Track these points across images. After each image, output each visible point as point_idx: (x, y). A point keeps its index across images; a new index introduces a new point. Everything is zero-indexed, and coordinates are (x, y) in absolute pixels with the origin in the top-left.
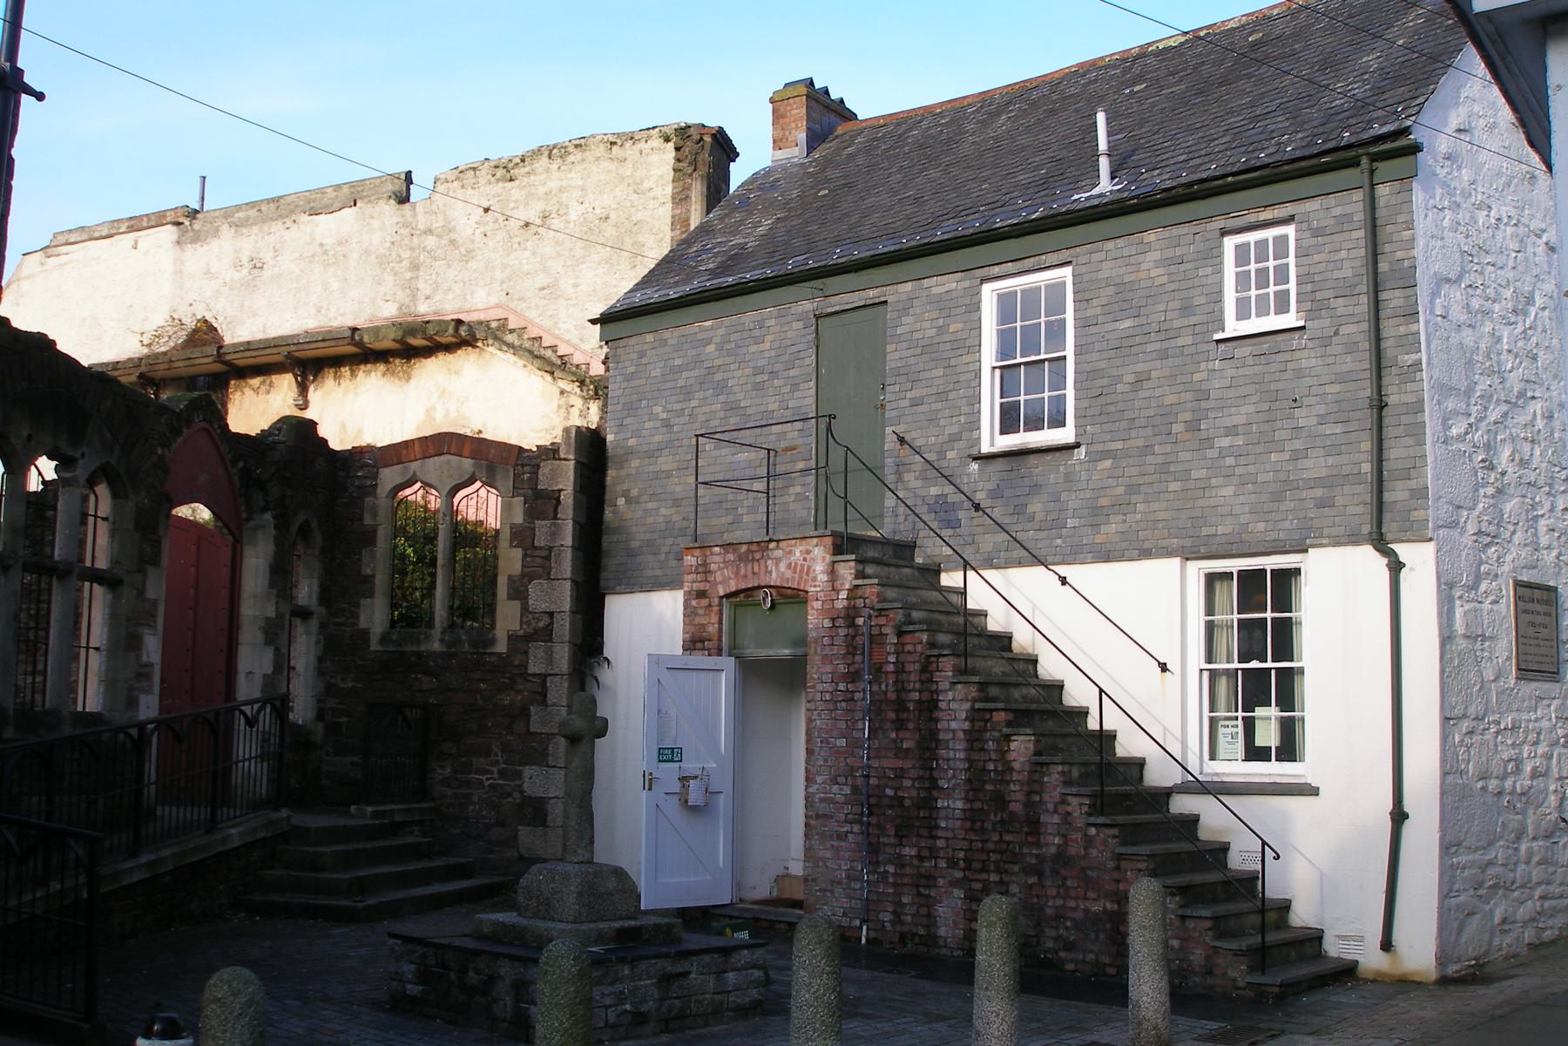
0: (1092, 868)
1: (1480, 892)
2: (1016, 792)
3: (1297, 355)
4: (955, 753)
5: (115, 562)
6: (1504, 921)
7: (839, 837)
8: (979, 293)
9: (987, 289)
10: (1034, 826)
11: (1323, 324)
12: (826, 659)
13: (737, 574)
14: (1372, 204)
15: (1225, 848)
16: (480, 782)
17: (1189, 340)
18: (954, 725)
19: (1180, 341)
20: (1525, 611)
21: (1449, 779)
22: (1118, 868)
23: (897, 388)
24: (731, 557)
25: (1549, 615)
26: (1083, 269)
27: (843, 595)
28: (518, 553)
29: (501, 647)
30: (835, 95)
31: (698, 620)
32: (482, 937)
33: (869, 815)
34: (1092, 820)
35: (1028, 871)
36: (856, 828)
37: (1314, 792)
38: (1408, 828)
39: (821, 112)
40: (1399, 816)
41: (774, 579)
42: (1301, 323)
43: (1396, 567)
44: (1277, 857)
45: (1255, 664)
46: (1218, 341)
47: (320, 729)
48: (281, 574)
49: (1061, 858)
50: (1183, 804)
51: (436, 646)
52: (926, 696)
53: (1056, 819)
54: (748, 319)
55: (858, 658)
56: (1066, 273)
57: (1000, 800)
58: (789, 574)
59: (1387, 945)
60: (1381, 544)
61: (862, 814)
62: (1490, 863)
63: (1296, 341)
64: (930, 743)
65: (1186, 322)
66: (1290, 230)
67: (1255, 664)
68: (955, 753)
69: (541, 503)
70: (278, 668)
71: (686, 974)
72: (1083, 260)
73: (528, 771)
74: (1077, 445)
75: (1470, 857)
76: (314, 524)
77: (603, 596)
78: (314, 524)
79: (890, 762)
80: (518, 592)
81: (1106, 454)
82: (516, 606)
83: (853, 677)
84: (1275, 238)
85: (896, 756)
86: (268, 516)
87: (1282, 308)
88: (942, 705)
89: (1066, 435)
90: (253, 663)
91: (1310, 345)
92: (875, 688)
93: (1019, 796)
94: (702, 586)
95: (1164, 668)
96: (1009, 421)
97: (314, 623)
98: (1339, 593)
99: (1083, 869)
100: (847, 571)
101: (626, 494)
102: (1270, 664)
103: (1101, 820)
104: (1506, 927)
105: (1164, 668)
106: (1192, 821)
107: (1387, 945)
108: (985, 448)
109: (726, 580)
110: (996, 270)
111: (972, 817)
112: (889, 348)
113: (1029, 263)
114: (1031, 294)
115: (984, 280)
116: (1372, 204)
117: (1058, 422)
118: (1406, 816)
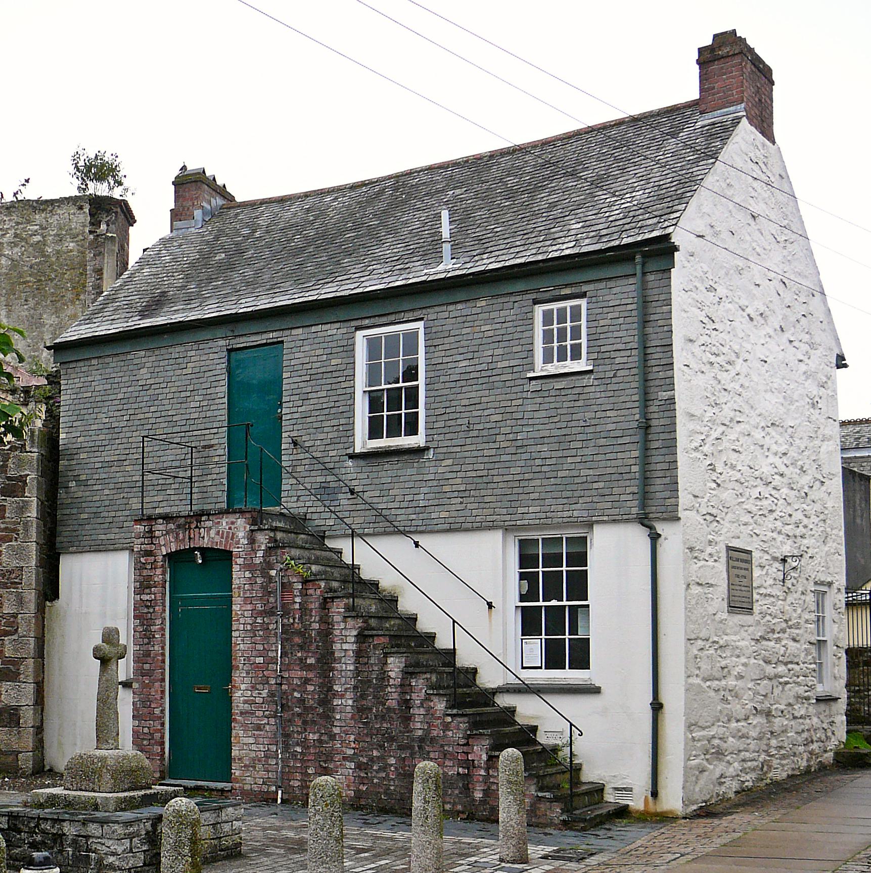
0: (449, 745)
1: (707, 757)
3: (586, 390)
4: (346, 666)
6: (721, 776)
9: (360, 334)
10: (407, 719)
12: (247, 600)
13: (177, 538)
14: (644, 286)
18: (345, 647)
20: (733, 567)
21: (690, 680)
22: (467, 744)
23: (291, 404)
25: (747, 569)
26: (431, 324)
27: (260, 554)
30: (709, 42)
31: (145, 573)
32: (41, 806)
33: (282, 712)
34: (449, 712)
35: (401, 748)
36: (272, 721)
37: (596, 691)
40: (657, 707)
41: (206, 543)
42: (591, 368)
43: (655, 538)
44: (581, 735)
45: (554, 603)
46: (531, 379)
50: (504, 701)
52: (324, 627)
53: (422, 711)
54: (176, 351)
55: (272, 600)
56: (420, 325)
58: (217, 539)
59: (655, 794)
60: (644, 520)
61: (276, 712)
62: (713, 737)
64: (327, 660)
66: (583, 303)
67: (554, 603)
68: (346, 666)
72: (431, 317)
74: (427, 449)
75: (702, 733)
77: (59, 554)
79: (297, 674)
84: (571, 307)
85: (302, 669)
87: (576, 355)
88: (337, 632)
89: (418, 440)
91: (596, 383)
92: (285, 621)
93: (395, 696)
94: (148, 547)
95: (490, 605)
96: (375, 432)
98: (614, 556)
99: (442, 746)
101: (76, 478)
102: (565, 603)
103: (455, 711)
104: (723, 780)
105: (490, 605)
106: (512, 711)
107: (655, 794)
109: (167, 544)
110: (366, 322)
111: (360, 710)
112: (285, 375)
113: (392, 318)
114: (392, 339)
115: (358, 328)
116: (644, 286)
117: (412, 430)
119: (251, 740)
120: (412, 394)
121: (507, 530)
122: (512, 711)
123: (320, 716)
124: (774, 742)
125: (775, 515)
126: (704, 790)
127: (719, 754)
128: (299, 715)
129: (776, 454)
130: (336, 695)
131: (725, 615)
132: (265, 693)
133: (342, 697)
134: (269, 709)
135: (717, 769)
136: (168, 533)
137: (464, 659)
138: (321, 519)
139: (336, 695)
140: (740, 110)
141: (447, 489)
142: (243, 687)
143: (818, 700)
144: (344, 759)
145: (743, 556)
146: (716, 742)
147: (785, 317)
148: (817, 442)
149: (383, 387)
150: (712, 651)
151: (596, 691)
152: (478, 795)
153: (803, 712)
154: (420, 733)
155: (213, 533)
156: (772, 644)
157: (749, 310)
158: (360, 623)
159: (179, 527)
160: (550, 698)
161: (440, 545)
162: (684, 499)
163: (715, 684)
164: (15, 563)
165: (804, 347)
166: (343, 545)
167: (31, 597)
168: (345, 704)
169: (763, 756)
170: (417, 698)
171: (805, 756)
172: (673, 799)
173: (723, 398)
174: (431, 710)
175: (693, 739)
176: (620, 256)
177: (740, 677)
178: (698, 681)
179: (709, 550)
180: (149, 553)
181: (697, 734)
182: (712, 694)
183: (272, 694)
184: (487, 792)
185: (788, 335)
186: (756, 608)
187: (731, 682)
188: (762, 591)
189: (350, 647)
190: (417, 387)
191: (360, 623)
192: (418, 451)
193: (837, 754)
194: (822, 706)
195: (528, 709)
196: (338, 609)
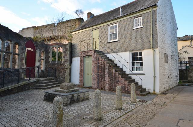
2: (113, 75)
4: (107, 71)
5: (18, 53)
10: (115, 78)
11: (145, 26)
15: (134, 80)
28: (64, 54)
29: (63, 62)
37: (144, 74)
39: (90, 14)
40: (155, 77)
47: (45, 70)
48: (40, 56)
49: (118, 81)
50: (130, 76)
51: (56, 62)
63: (143, 28)
64: (104, 70)
68: (107, 71)
69: (66, 49)
70: (40, 64)
71: (80, 95)
76: (44, 51)
78: (44, 51)
79: (100, 72)
80: (64, 57)
82: (64, 59)
83: (96, 64)
86: (39, 50)
90: (37, 64)
95: (127, 62)
97: (44, 61)
98: (147, 55)
100: (96, 53)
105: (127, 62)
106: (131, 77)
108: (109, 42)
111: (109, 77)
118: (155, 77)
121: (130, 51)
122: (131, 77)
124: (171, 82)
126: (163, 90)
127: (164, 84)
131: (164, 63)
137: (124, 70)
138: (104, 51)
146: (164, 82)
151: (144, 74)
152: (126, 89)
158: (109, 65)
160: (137, 75)
161: (120, 54)
162: (159, 45)
163: (163, 73)
166: (107, 55)
168: (107, 75)
169: (169, 84)
170: (117, 75)
172: (158, 91)
174: (119, 77)
179: (162, 53)
180: (81, 56)
181: (161, 81)
183: (97, 75)
184: (128, 89)
187: (166, 73)
189: (107, 68)
191: (109, 65)
195: (133, 77)
196: (106, 62)
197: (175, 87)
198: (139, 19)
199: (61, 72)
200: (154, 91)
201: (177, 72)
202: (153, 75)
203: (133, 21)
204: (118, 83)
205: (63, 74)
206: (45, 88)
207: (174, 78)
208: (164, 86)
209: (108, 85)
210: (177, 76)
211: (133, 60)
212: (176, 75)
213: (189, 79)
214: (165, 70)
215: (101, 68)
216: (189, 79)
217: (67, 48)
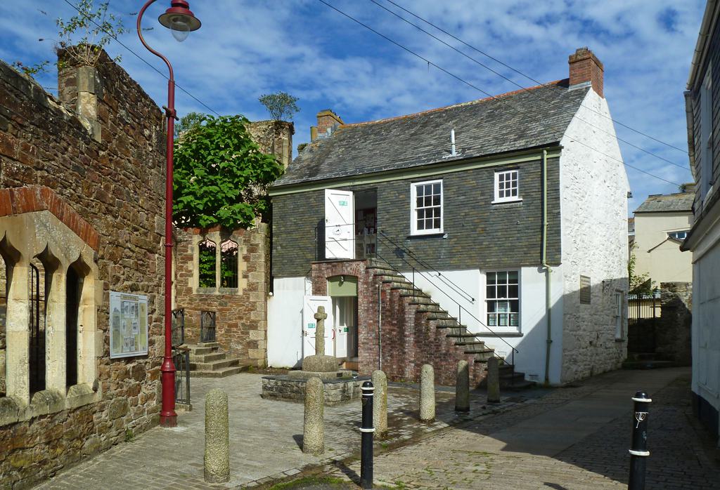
4: (410, 324)
6: (576, 371)
7: (371, 349)
8: (410, 186)
10: (438, 346)
16: (235, 336)
17: (483, 203)
18: (410, 316)
19: (480, 204)
24: (330, 266)
27: (371, 278)
31: (318, 285)
38: (552, 346)
40: (549, 342)
42: (521, 199)
45: (502, 299)
56: (441, 181)
57: (427, 337)
65: (482, 198)
67: (502, 299)
68: (410, 324)
73: (251, 332)
77: (307, 275)
79: (388, 327)
81: (455, 237)
89: (440, 231)
98: (530, 279)
106: (482, 343)
111: (417, 342)
114: (429, 226)
119: (367, 354)
120: (438, 212)
123: (399, 344)
124: (597, 358)
125: (600, 262)
126: (570, 377)
127: (575, 362)
128: (389, 344)
129: (601, 236)
130: (405, 336)
131: (579, 304)
132: (374, 335)
133: (409, 337)
134: (375, 341)
135: (574, 368)
136: (328, 268)
139: (405, 336)
140: (589, 84)
141: (454, 251)
142: (363, 332)
143: (616, 341)
144: (410, 362)
145: (587, 279)
146: (574, 357)
147: (606, 176)
148: (618, 231)
149: (432, 206)
150: (573, 319)
153: (610, 345)
154: (444, 351)
155: (349, 269)
156: (597, 316)
157: (592, 174)
159: (333, 266)
163: (574, 333)
164: (255, 281)
165: (614, 189)
167: (262, 294)
169: (593, 364)
171: (610, 364)
172: (555, 379)
173: (580, 212)
175: (565, 355)
176: (537, 150)
177: (584, 330)
178: (568, 331)
179: (573, 277)
182: (573, 337)
185: (607, 184)
186: (592, 301)
187: (581, 332)
188: (594, 294)
189: (412, 316)
190: (440, 208)
192: (440, 236)
193: (623, 364)
194: (618, 344)
197: (611, 371)
198: (509, 174)
199: (236, 326)
200: (547, 379)
201: (622, 327)
202: (546, 338)
203: (493, 180)
204: (446, 360)
205: (242, 333)
206: (219, 374)
207: (609, 344)
208: (574, 368)
209: (413, 365)
210: (623, 341)
211: (490, 292)
212: (618, 336)
213: (659, 349)
214: (581, 324)
215: (392, 315)
216: (659, 349)
217: (257, 245)
